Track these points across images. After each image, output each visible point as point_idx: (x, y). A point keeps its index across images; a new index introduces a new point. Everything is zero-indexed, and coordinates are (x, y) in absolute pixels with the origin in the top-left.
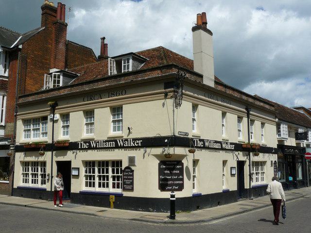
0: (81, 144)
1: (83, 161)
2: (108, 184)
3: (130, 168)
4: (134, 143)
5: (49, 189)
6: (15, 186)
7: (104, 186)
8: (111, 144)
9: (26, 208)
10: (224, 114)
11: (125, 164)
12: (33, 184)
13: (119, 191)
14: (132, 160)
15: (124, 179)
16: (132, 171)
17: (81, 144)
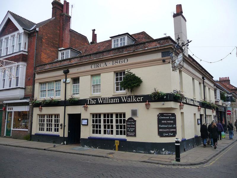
0: (90, 101)
1: (91, 114)
2: (100, 131)
3: (132, 119)
4: (136, 99)
5: (62, 135)
6: (33, 133)
7: (97, 133)
8: (115, 100)
9: (46, 151)
10: (193, 79)
11: (128, 116)
12: (48, 132)
13: (123, 137)
14: (134, 113)
15: (127, 127)
16: (135, 121)
17: (90, 101)
